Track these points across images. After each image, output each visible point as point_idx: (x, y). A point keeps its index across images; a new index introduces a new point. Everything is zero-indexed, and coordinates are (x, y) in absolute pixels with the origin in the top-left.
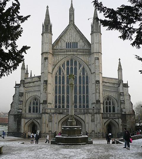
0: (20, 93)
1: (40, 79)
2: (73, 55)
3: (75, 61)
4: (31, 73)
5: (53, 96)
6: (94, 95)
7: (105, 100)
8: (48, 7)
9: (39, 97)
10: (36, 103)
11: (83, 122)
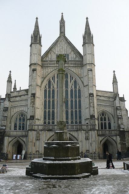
1: (27, 92)
4: (15, 83)
10: (23, 119)
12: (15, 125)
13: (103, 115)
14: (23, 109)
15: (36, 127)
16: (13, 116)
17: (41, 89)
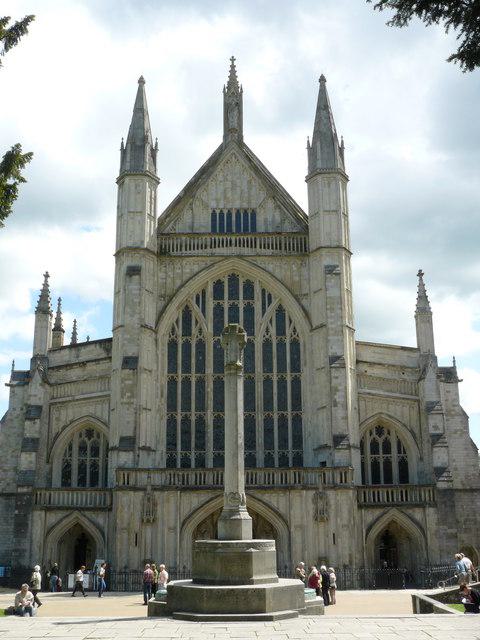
0: (29, 406)
1: (108, 350)
2: (240, 257)
6: (323, 415)
7: (368, 435)
8: (141, 81)
13: (380, 430)
16: (58, 435)
17: (156, 340)
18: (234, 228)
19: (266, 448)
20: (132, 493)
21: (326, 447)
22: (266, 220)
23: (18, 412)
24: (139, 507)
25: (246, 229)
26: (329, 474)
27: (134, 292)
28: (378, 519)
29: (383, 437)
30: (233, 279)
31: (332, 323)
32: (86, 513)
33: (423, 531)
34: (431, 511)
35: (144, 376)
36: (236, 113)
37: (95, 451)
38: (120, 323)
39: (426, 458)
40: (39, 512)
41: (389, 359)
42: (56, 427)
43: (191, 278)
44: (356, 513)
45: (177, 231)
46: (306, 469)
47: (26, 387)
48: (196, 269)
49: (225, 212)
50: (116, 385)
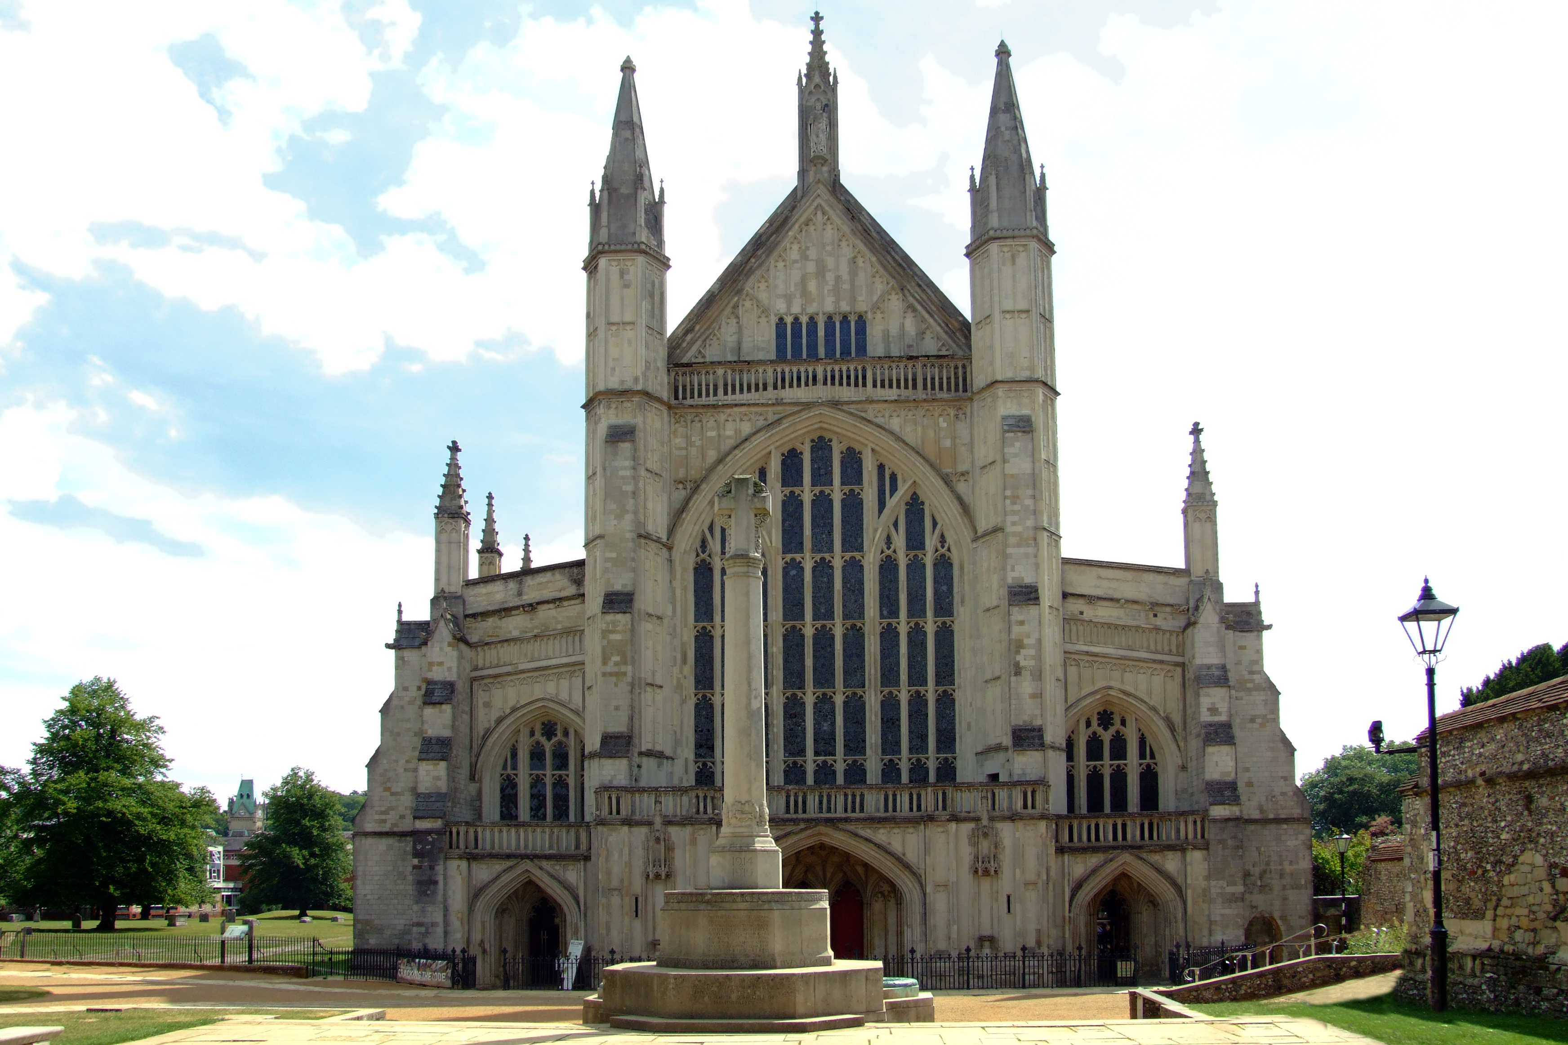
0: (429, 682)
1: (579, 582)
2: (835, 404)
3: (850, 449)
4: (490, 512)
5: (684, 701)
6: (995, 692)
7: (1083, 724)
8: (628, 68)
9: (576, 712)
10: (555, 755)
11: (905, 883)
12: (502, 790)
13: (1105, 718)
14: (551, 688)
15: (645, 804)
16: (488, 733)
17: (670, 561)
18: (821, 351)
19: (884, 752)
20: (625, 829)
21: (999, 748)
22: (886, 336)
23: (413, 692)
24: (640, 852)
25: (845, 352)
26: (1002, 795)
27: (622, 473)
28: (1094, 872)
29: (1112, 730)
30: (821, 446)
31: (1014, 524)
32: (545, 864)
33: (1179, 891)
34: (1196, 857)
35: (647, 627)
36: (823, 125)
37: (561, 759)
38: (597, 532)
39: (1191, 766)
40: (456, 863)
41: (1128, 589)
42: (484, 719)
43: (736, 447)
44: (1053, 861)
45: (708, 360)
46: (958, 787)
47: (424, 648)
48: (746, 428)
49: (804, 320)
50: (593, 644)
